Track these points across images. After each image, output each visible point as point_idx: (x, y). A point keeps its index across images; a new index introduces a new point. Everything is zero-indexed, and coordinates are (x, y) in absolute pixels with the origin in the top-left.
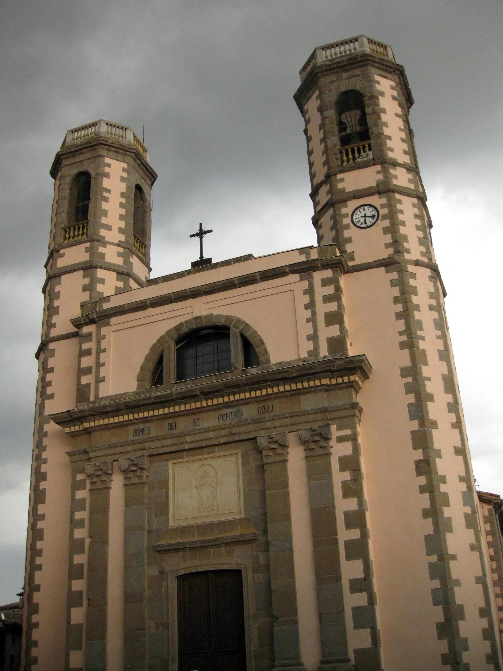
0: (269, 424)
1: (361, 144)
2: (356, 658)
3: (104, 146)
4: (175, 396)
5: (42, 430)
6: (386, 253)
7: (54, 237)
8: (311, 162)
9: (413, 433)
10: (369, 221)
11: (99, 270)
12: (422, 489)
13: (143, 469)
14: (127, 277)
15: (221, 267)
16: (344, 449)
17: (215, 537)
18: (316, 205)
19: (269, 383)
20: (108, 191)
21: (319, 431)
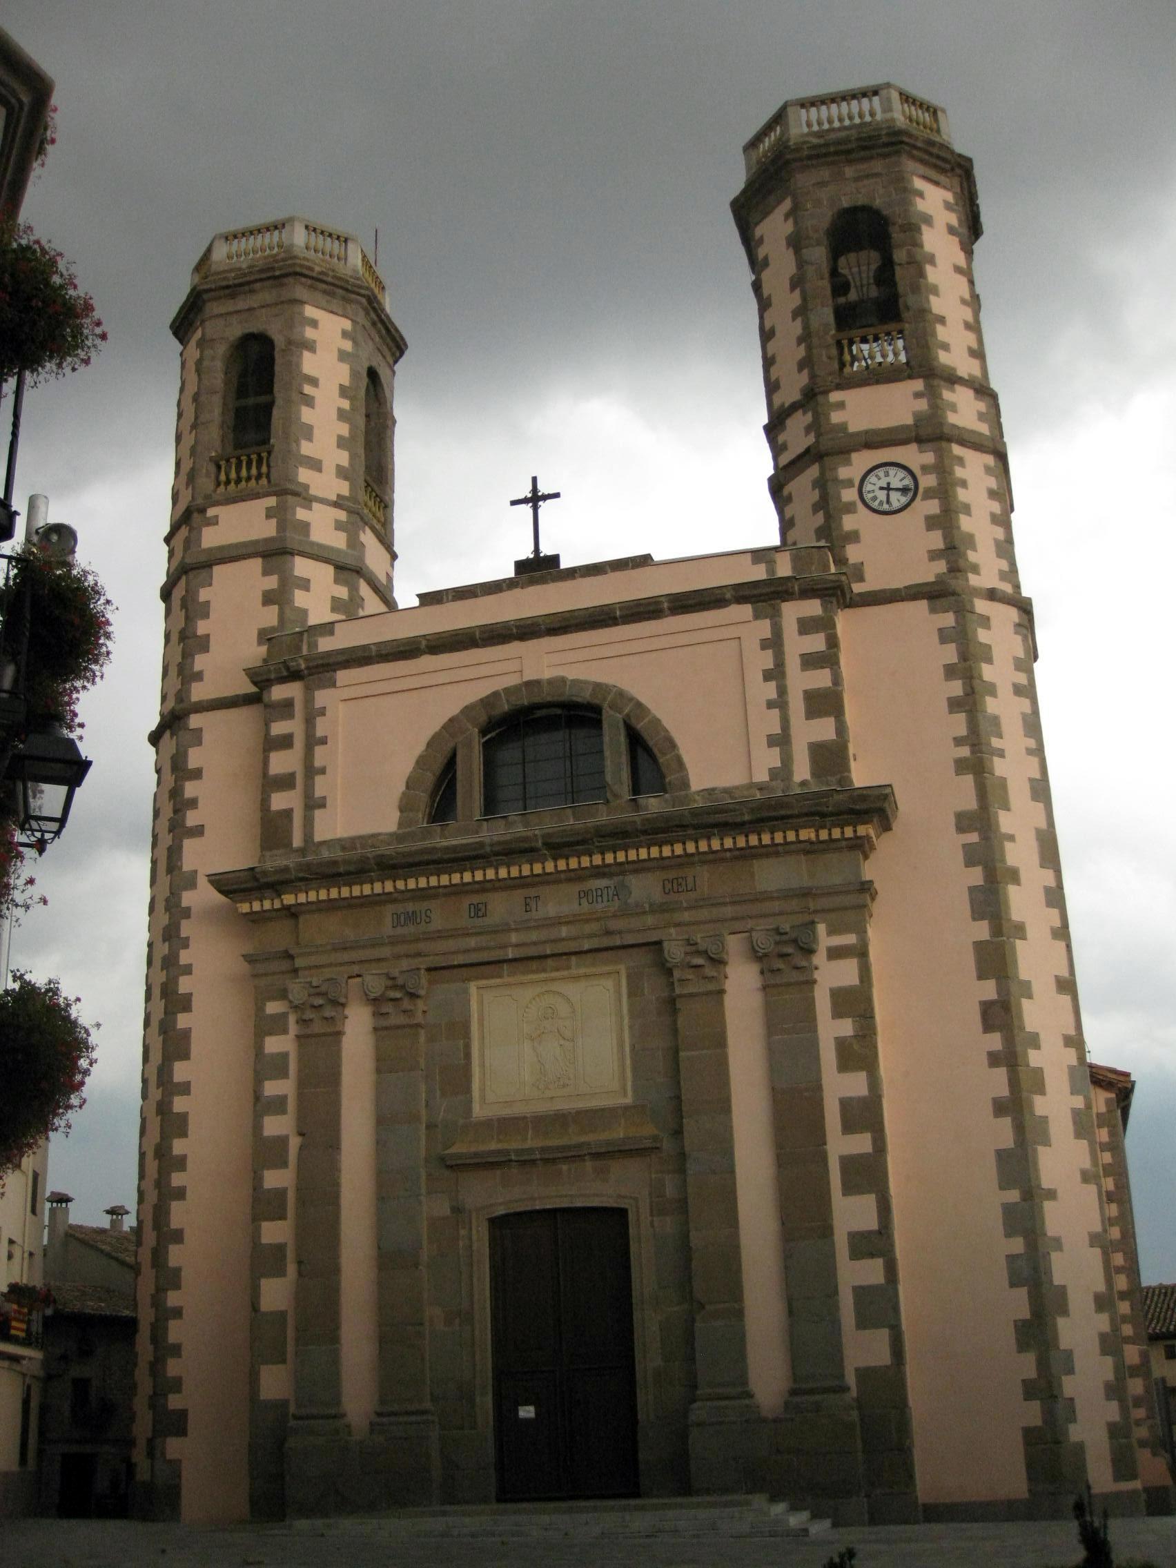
0: (686, 916)
3: (303, 280)
5: (178, 904)
6: (929, 572)
8: (769, 355)
9: (979, 946)
10: (897, 500)
12: (994, 1059)
13: (418, 997)
14: (354, 575)
15: (583, 576)
16: (844, 973)
17: (573, 1142)
18: (777, 450)
20: (314, 382)
21: (794, 936)
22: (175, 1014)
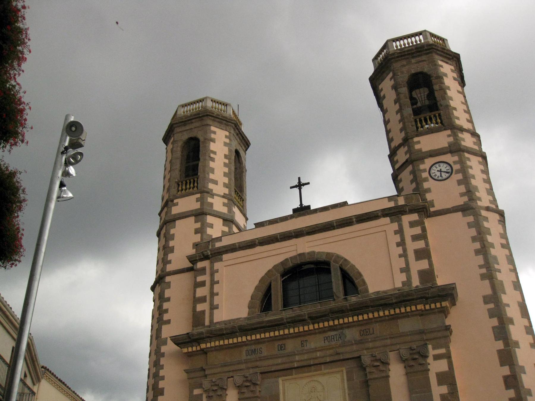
0: (371, 345)
1: (432, 114)
4: (285, 320)
6: (462, 201)
7: (167, 189)
8: (388, 129)
9: (499, 352)
11: (208, 217)
13: (257, 384)
15: (320, 212)
16: (442, 366)
19: (371, 309)
20: (215, 153)
22: (157, 396)
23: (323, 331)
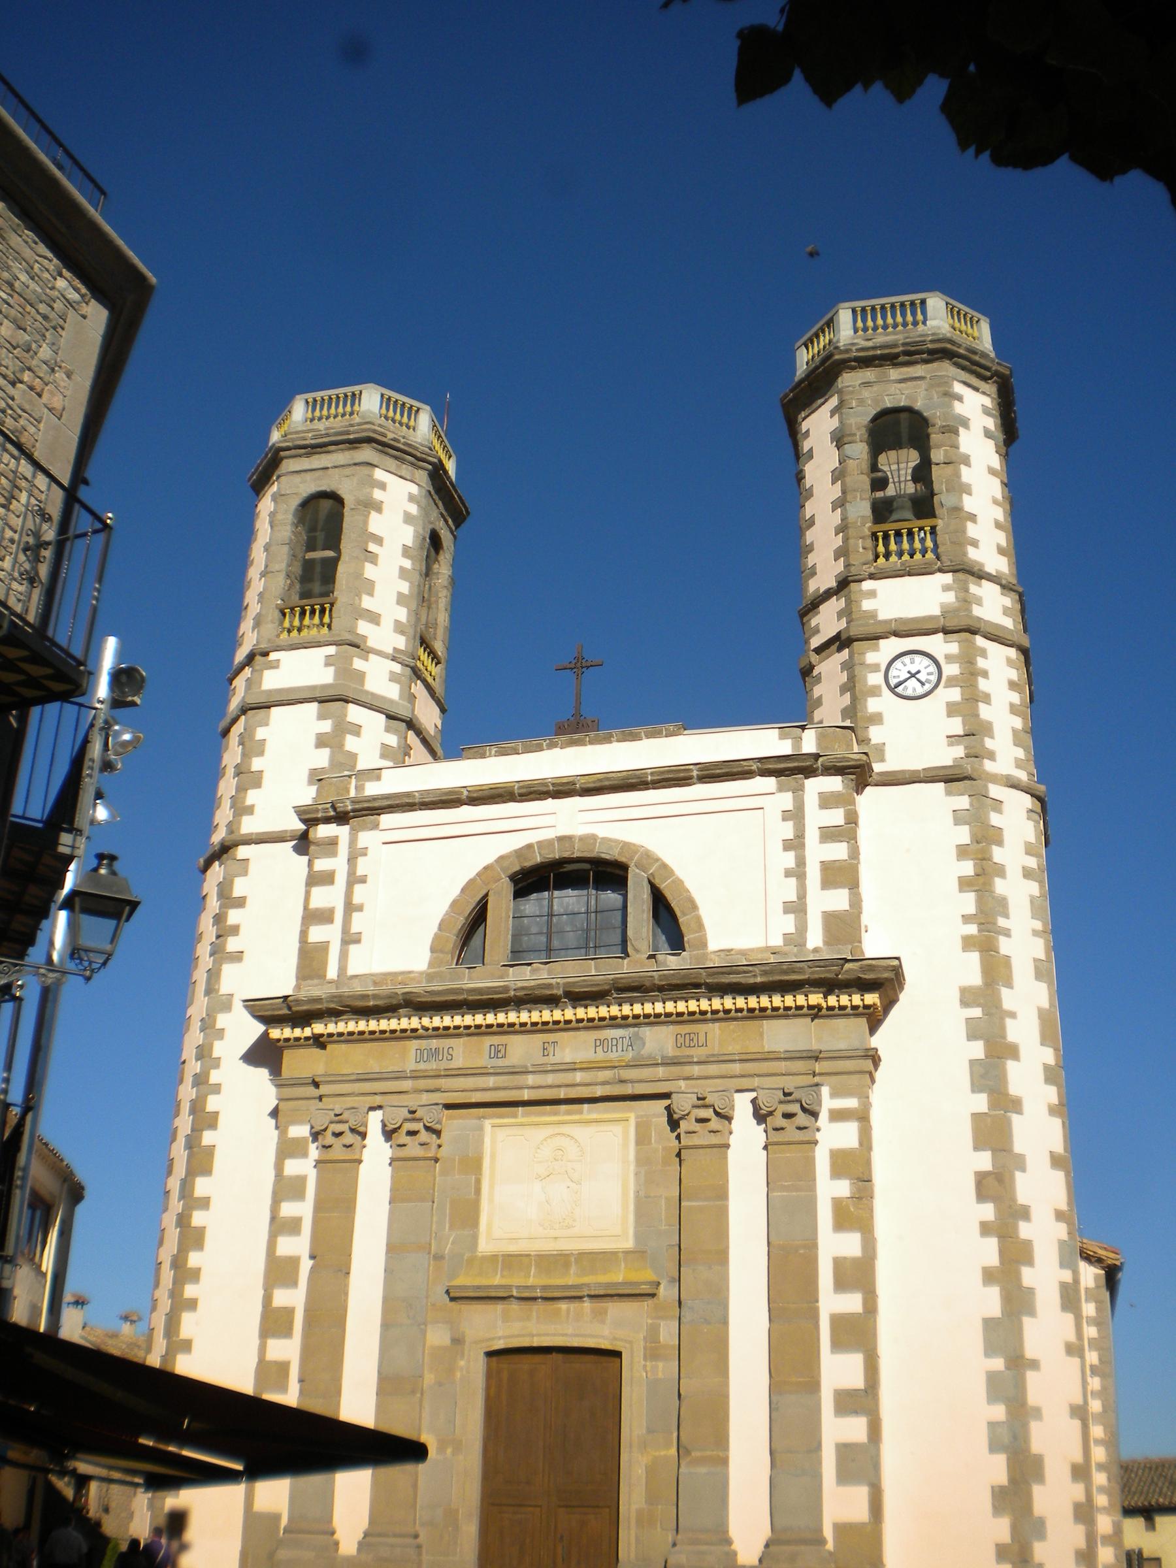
1: (915, 524)
2: (836, 1538)
4: (512, 993)
6: (948, 756)
20: (379, 540)
23: (592, 1024)
